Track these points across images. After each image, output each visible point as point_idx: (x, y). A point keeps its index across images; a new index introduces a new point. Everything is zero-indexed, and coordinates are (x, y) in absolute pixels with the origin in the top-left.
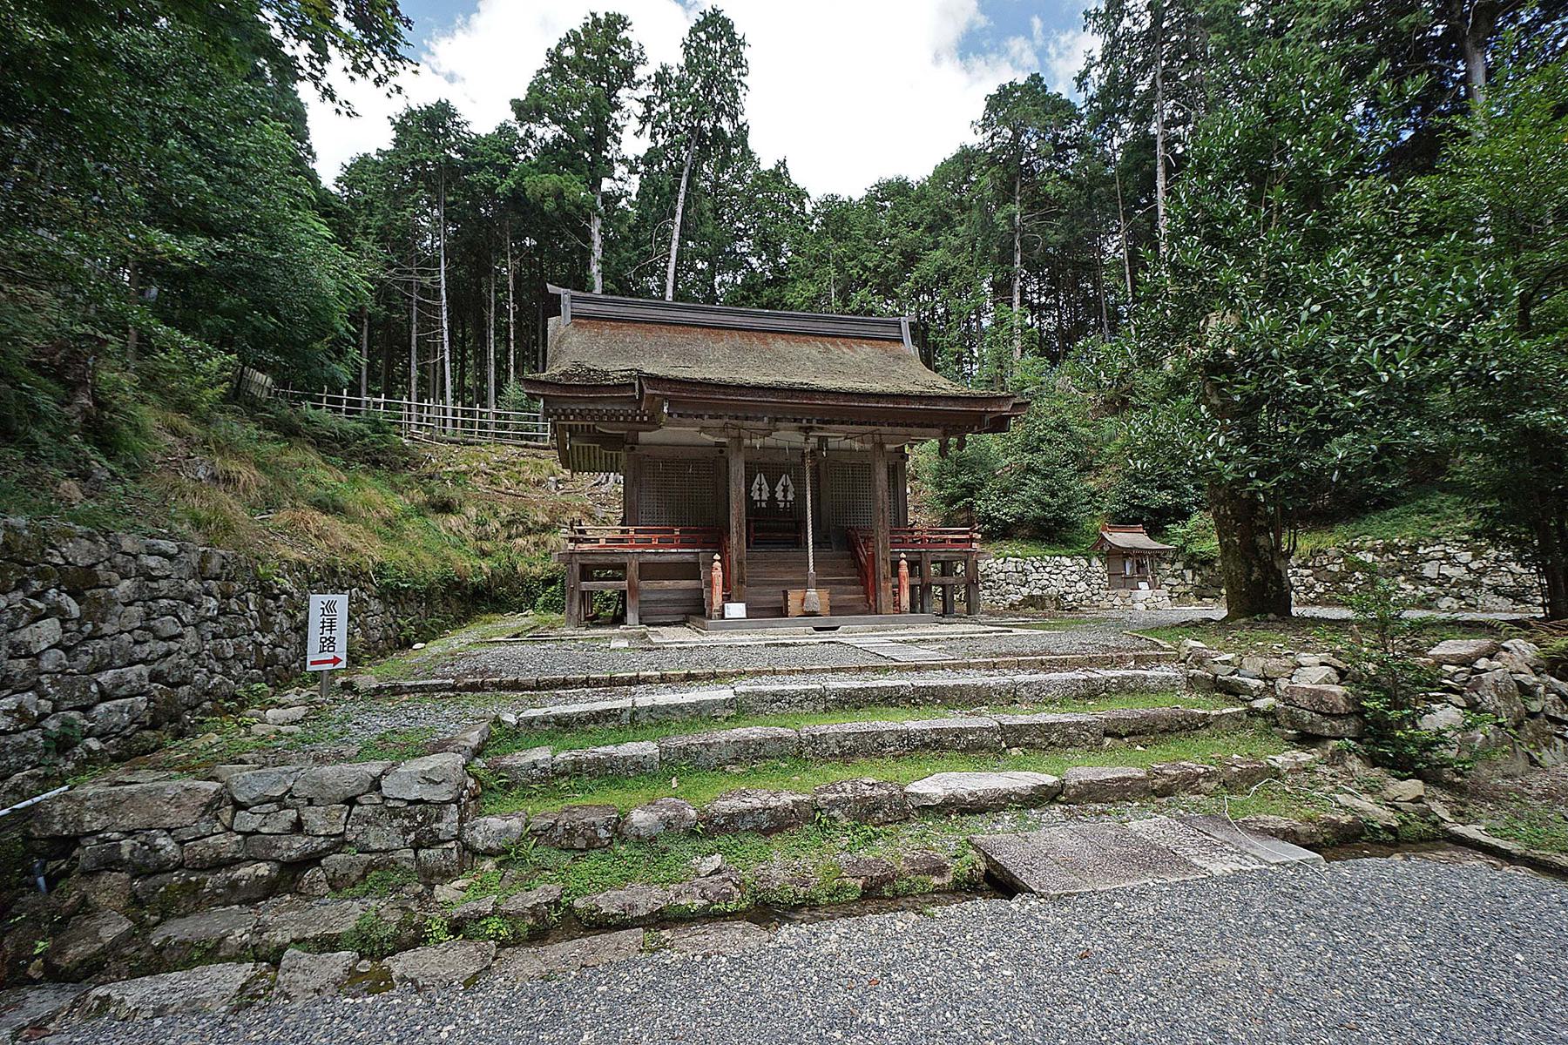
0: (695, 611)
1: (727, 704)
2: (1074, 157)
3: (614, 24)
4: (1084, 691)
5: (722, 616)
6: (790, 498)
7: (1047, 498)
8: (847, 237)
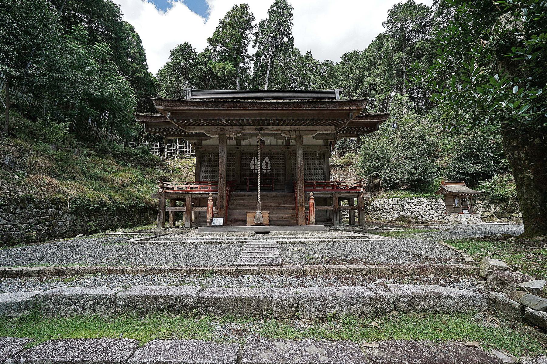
0: (200, 222)
1: (22, 306)
2: (430, 29)
3: (245, 7)
4: (369, 309)
5: (211, 225)
6: (269, 168)
7: (413, 170)
8: (334, 76)
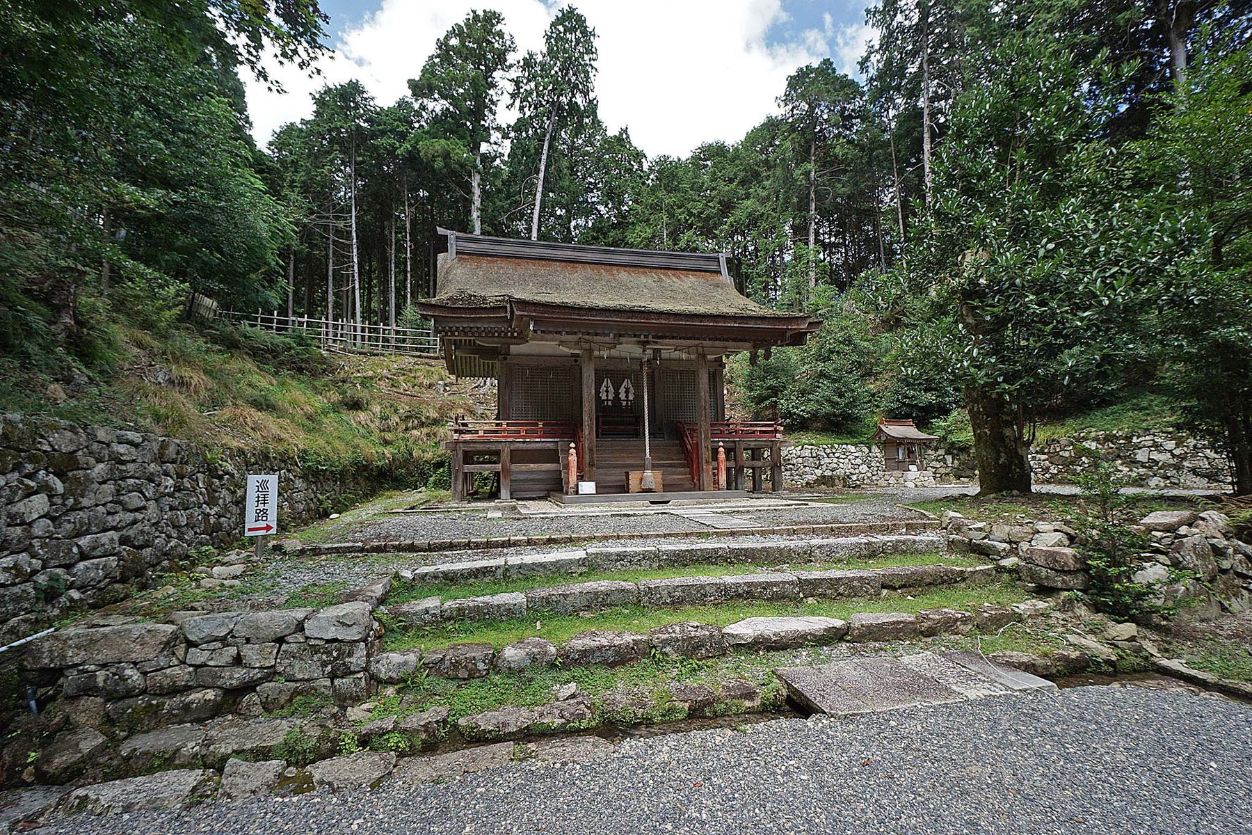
0: (555, 488)
1: (581, 562)
2: (858, 125)
3: (490, 19)
4: (865, 552)
5: (577, 493)
6: (631, 398)
7: (836, 398)
8: (676, 189)
